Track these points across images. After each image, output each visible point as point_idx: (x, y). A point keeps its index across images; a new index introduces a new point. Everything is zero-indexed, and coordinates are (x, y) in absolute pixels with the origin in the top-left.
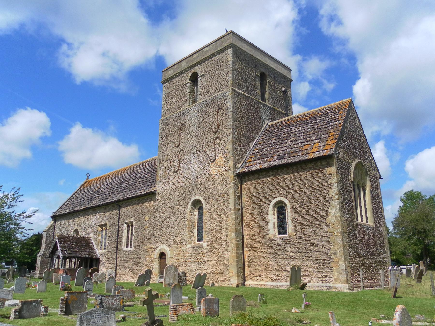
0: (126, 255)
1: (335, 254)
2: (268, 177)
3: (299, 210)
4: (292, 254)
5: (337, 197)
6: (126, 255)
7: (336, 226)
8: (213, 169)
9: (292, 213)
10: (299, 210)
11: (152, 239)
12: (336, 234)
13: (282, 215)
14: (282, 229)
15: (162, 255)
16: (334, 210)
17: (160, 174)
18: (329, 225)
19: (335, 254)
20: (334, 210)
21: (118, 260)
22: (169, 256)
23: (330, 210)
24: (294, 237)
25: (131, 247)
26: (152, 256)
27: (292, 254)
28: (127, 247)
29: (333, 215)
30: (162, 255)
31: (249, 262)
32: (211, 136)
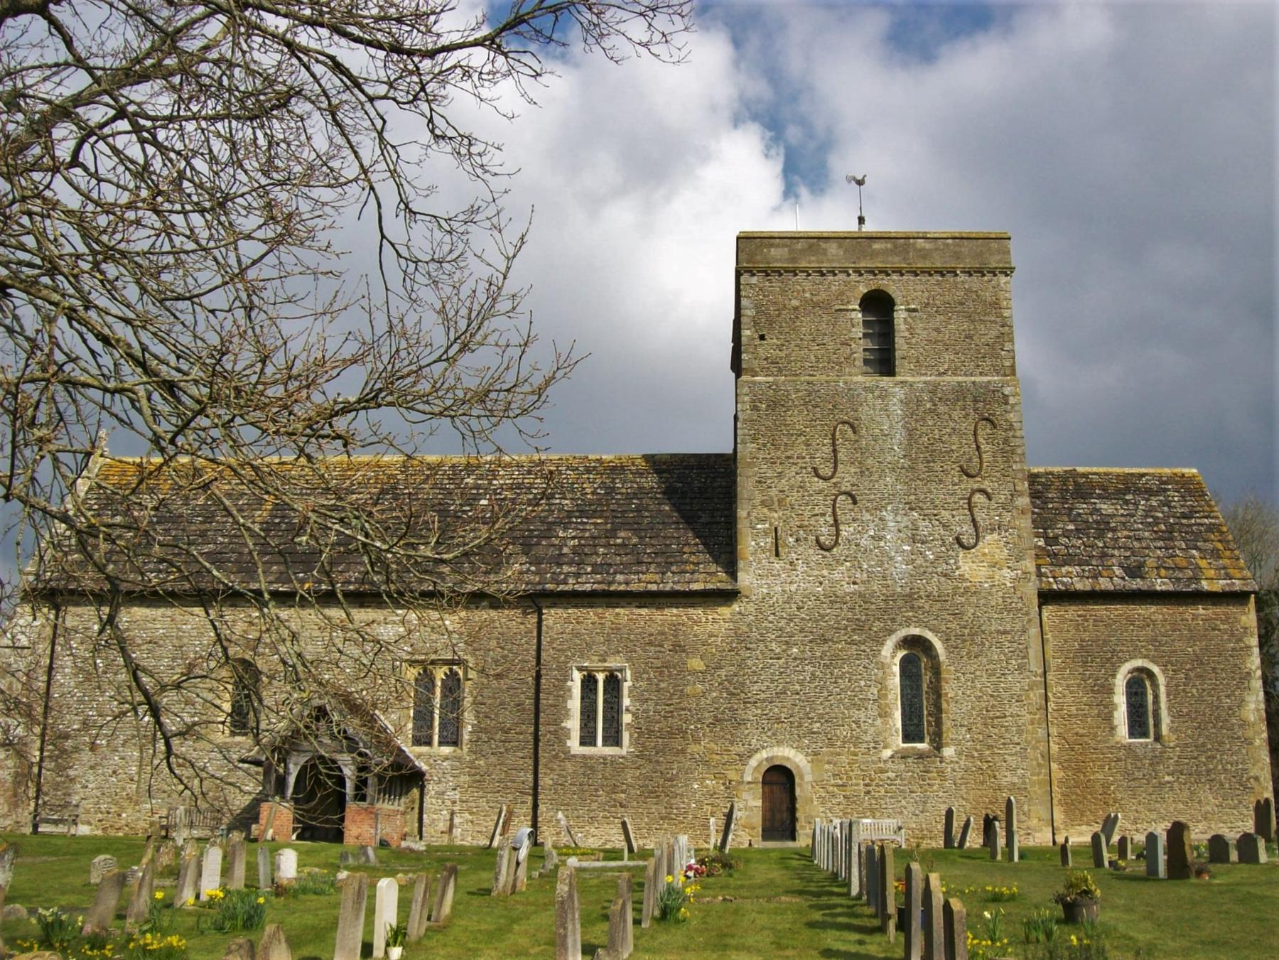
0: (591, 768)
1: (1257, 779)
2: (576, 606)
3: (1184, 691)
4: (1167, 778)
5: (1259, 673)
6: (591, 768)
7: (1257, 728)
8: (969, 567)
9: (1168, 695)
10: (1184, 691)
11: (727, 723)
12: (1257, 742)
13: (1136, 694)
14: (1138, 724)
15: (780, 780)
16: (1254, 698)
17: (341, 925)
18: (1244, 724)
19: (1257, 779)
20: (1254, 698)
21: (545, 781)
22: (808, 778)
23: (1248, 698)
24: (1172, 745)
25: (613, 738)
26: (732, 775)
27: (1167, 778)
28: (588, 739)
29: (1252, 706)
30: (780, 780)
31: (1063, 795)
32: (955, 485)
